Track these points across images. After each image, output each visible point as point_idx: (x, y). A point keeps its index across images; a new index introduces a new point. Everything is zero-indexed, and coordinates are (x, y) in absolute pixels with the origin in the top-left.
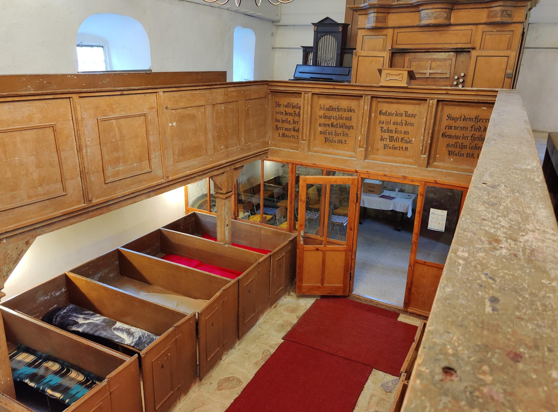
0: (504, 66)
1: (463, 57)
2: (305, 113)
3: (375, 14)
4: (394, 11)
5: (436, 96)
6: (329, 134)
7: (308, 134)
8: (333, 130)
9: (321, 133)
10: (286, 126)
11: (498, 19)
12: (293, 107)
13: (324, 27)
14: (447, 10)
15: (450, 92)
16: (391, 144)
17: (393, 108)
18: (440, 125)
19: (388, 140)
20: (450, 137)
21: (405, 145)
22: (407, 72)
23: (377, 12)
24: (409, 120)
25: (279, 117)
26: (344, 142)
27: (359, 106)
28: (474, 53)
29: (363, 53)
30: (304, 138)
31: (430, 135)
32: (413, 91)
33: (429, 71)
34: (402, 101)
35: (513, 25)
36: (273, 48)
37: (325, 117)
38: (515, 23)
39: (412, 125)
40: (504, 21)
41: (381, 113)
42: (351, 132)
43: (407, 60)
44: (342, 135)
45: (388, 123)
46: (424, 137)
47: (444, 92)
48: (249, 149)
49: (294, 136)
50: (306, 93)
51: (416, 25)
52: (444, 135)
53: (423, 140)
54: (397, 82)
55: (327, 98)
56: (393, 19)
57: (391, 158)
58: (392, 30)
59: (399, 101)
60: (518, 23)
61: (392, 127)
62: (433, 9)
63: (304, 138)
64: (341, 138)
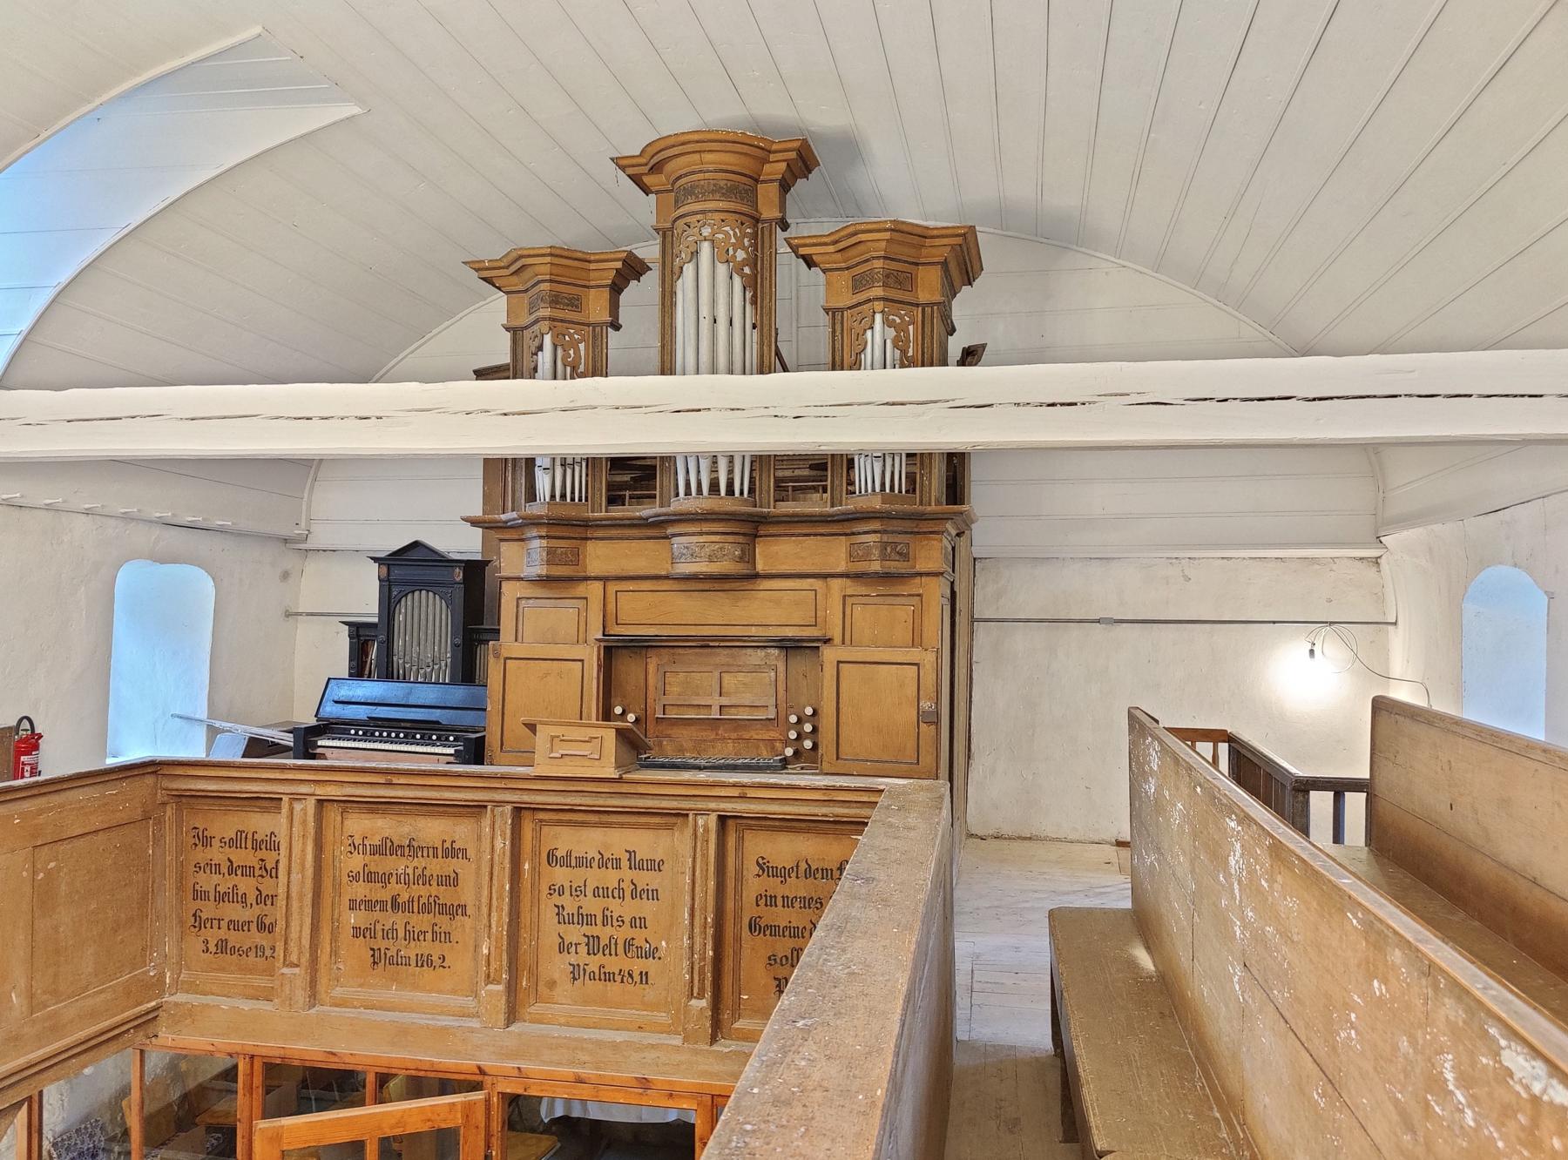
0: (911, 690)
1: (800, 663)
2: (295, 867)
3: (544, 542)
4: (600, 533)
5: (713, 805)
6: (385, 936)
7: (306, 942)
8: (399, 919)
9: (358, 932)
10: (234, 912)
11: (876, 566)
12: (257, 846)
13: (408, 568)
14: (741, 539)
15: (751, 793)
16: (593, 963)
17: (587, 842)
18: (738, 893)
19: (583, 949)
20: (774, 930)
21: (637, 966)
22: (613, 733)
23: (548, 537)
24: (645, 879)
25: (207, 881)
26: (437, 962)
27: (479, 838)
28: (829, 654)
29: (517, 650)
30: (294, 958)
31: (710, 931)
32: (641, 789)
33: (716, 701)
34: (613, 819)
35: (917, 580)
36: (288, 615)
37: (370, 877)
38: (921, 574)
39: (654, 895)
40: (893, 570)
41: (551, 857)
42: (463, 927)
43: (651, 668)
44: (429, 936)
45: (578, 891)
46: (691, 937)
47: (735, 792)
48: (56, 1029)
49: (259, 950)
50: (296, 798)
51: (663, 573)
52: (754, 926)
53: (692, 948)
54: (587, 763)
55: (372, 811)
56: (600, 556)
57: (595, 1012)
58: (598, 585)
59: (605, 818)
60: (928, 574)
61: (592, 905)
62: (701, 534)
63: (294, 958)
64: (425, 947)
